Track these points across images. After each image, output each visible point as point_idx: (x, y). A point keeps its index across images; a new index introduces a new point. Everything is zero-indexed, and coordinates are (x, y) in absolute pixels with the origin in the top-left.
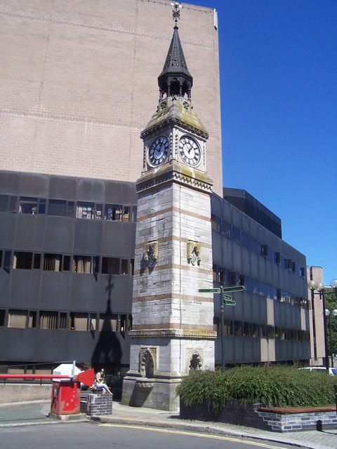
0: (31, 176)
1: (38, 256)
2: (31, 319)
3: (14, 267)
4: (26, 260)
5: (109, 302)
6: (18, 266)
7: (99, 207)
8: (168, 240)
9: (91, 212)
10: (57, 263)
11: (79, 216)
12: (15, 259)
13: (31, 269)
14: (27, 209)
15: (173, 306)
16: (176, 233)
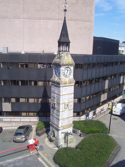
0: (12, 115)
1: (27, 81)
2: (27, 99)
3: (20, 85)
4: (24, 83)
5: (65, 18)
6: (21, 85)
7: (45, 64)
8: (59, 104)
9: (43, 66)
10: (33, 82)
11: (39, 68)
12: (20, 82)
13: (25, 85)
14: (22, 66)
15: (60, 122)
16: (61, 102)
